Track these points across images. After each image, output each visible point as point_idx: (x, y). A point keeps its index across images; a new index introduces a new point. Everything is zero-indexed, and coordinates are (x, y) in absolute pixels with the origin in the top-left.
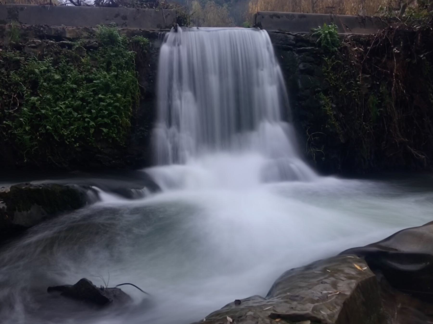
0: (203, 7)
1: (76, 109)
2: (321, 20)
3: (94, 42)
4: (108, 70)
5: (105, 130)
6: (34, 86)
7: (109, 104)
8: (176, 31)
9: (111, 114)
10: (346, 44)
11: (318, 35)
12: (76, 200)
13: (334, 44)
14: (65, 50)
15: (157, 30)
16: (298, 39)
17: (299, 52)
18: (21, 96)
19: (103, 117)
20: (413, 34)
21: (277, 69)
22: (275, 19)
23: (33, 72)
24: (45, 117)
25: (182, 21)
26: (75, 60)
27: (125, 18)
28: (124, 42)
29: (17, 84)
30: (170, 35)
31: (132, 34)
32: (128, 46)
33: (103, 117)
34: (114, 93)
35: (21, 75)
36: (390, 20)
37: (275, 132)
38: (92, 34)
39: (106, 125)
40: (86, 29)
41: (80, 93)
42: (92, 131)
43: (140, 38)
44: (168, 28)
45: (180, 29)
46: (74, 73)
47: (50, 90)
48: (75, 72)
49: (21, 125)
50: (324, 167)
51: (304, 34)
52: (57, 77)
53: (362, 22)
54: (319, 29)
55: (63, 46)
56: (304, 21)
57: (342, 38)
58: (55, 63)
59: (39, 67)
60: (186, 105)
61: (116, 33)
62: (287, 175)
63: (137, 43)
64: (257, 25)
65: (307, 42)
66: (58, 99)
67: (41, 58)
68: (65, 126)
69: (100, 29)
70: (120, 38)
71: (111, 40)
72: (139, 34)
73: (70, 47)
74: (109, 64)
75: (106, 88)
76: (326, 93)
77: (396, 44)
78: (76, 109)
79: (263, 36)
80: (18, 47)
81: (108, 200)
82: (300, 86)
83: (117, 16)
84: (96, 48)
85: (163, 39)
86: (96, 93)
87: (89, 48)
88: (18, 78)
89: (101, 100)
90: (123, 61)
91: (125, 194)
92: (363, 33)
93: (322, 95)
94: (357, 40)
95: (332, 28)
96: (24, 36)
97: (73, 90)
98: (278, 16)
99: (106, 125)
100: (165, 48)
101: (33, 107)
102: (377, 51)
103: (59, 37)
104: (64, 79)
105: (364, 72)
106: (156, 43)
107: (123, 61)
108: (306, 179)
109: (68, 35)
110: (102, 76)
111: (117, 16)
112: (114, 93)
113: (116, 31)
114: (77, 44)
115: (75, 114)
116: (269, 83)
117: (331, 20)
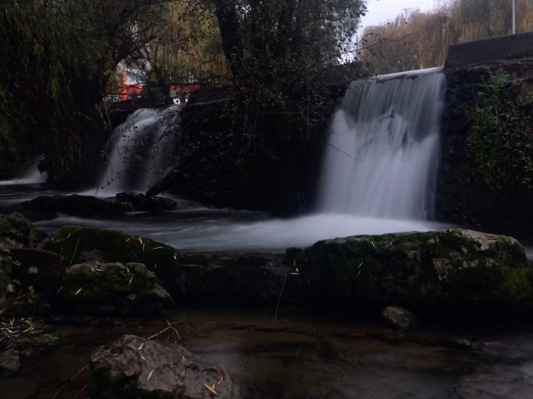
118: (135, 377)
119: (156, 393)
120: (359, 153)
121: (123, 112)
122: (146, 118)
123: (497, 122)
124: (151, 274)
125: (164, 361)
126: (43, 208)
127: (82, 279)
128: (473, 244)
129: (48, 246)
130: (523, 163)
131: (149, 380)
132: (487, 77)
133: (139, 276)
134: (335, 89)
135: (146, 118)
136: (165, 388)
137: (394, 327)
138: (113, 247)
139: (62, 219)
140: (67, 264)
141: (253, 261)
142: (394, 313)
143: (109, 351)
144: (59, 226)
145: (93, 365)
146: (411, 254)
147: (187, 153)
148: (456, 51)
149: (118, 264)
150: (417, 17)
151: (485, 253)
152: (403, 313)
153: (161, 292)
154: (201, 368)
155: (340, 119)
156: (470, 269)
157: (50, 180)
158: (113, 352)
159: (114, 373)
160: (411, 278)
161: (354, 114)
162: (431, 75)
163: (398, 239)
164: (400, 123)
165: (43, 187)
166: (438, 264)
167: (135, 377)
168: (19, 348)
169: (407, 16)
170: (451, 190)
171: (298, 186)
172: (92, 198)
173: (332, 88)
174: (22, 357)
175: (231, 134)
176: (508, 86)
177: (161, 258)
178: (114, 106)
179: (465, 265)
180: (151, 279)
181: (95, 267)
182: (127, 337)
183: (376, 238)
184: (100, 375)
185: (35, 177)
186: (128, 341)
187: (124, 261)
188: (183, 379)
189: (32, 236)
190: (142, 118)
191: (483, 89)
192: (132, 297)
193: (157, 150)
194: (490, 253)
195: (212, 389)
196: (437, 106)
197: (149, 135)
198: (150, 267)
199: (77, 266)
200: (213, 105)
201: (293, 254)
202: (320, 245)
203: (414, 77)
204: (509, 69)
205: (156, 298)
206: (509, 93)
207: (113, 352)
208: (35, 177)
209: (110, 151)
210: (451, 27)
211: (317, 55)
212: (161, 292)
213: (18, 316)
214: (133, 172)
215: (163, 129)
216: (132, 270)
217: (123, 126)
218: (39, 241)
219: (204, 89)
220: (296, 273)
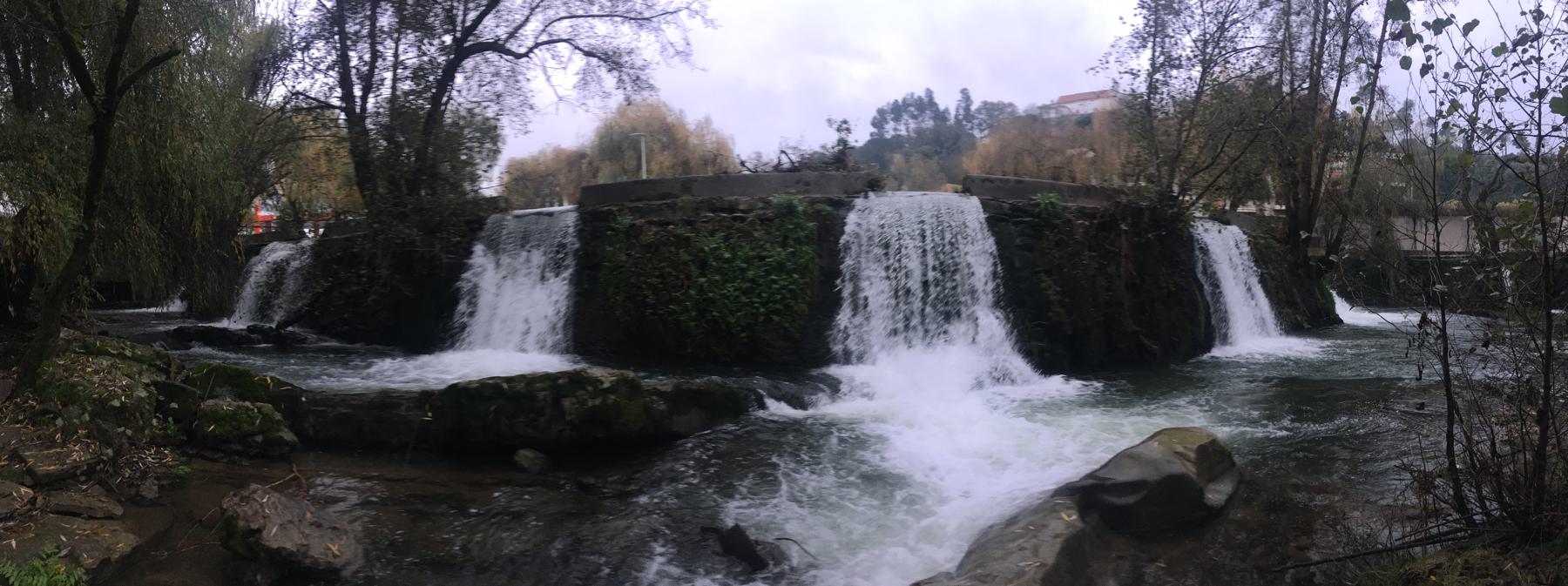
0: (907, 161)
1: (745, 292)
2: (1041, 188)
3: (770, 213)
4: (784, 245)
5: (776, 318)
6: (703, 266)
7: (783, 287)
8: (866, 197)
9: (784, 298)
10: (1070, 216)
11: (1038, 205)
12: (736, 406)
13: (1056, 215)
14: (737, 225)
15: (843, 196)
16: (1014, 208)
17: (1016, 224)
18: (688, 277)
19: (775, 302)
20: (1140, 210)
21: (990, 244)
22: (988, 184)
23: (702, 250)
24: (712, 301)
25: (875, 185)
26: (747, 235)
27: (807, 184)
28: (804, 212)
29: (686, 263)
30: (859, 202)
31: (813, 202)
32: (809, 216)
33: (775, 302)
34: (789, 273)
35: (690, 254)
36: (1120, 191)
37: (992, 324)
38: (768, 203)
39: (777, 312)
40: (762, 200)
41: (750, 274)
42: (761, 318)
43: (823, 206)
44: (856, 194)
45: (871, 194)
46: (746, 250)
47: (719, 271)
48: (747, 249)
49: (686, 310)
50: (1046, 366)
51: (1021, 202)
52: (727, 255)
53: (1088, 191)
54: (1038, 198)
55: (735, 219)
56: (1020, 188)
57: (1065, 208)
58: (726, 239)
59: (710, 244)
60: (876, 289)
61: (796, 202)
62: (1002, 377)
63: (819, 212)
64: (967, 191)
65: (1026, 213)
66: (726, 281)
67: (712, 234)
68: (732, 313)
69: (776, 199)
70: (800, 208)
71: (790, 209)
72: (821, 201)
73: (743, 219)
74: (786, 238)
75: (780, 268)
76: (1048, 273)
77: (1124, 220)
78: (745, 292)
79: (975, 201)
80: (689, 223)
81: (778, 409)
82: (1017, 264)
83: (798, 182)
84: (770, 220)
85: (850, 207)
86: (768, 273)
87: (764, 221)
88: (686, 257)
89: (774, 282)
90: (802, 234)
91: (799, 403)
92: (1089, 204)
93: (1043, 277)
94: (1082, 213)
95: (1053, 197)
96: (696, 210)
97: (743, 270)
98: (992, 181)
99: (777, 312)
100: (852, 218)
101: (701, 290)
102: (1104, 225)
103: (732, 209)
104: (735, 257)
105: (1091, 249)
106: (841, 213)
107: (802, 234)
108: (1027, 382)
109: (742, 207)
110: (777, 253)
111: (798, 182)
112: (789, 273)
113: (796, 199)
114: (751, 216)
115: (744, 299)
116: (979, 258)
117: (1052, 188)
118: (259, 531)
119: (280, 550)
120: (499, 286)
121: (255, 247)
122: (278, 251)
123: (624, 258)
124: (278, 416)
125: (288, 517)
126: (182, 338)
127: (215, 417)
128: (597, 382)
129: (187, 380)
130: (646, 297)
131: (274, 537)
132: (615, 219)
133: (266, 418)
134: (472, 222)
135: (278, 251)
136: (288, 546)
137: (525, 470)
138: (241, 383)
139: (198, 349)
140: (202, 399)
141: (387, 401)
142: (525, 456)
143: (237, 499)
144: (196, 357)
145: (224, 511)
146: (541, 395)
147: (319, 290)
148: (587, 191)
149: (247, 404)
150: (558, 153)
151: (607, 391)
152: (882, 426)
153: (288, 436)
154: (326, 525)
155: (479, 249)
156: (594, 407)
157: (189, 308)
158: (241, 500)
159: (241, 523)
160: (542, 419)
161: (494, 247)
162: (566, 212)
163: (529, 380)
164: (538, 258)
165: (182, 316)
166: (567, 403)
167: (259, 531)
168: (158, 478)
169: (549, 151)
170: (584, 329)
171: (434, 319)
172: (225, 330)
173: (468, 223)
174: (161, 488)
175: (14, 543)
176: (632, 226)
177: (289, 400)
178: (251, 237)
179: (590, 403)
180: (278, 422)
181: (227, 404)
182: (254, 486)
183: (508, 380)
184: (228, 525)
185: (176, 306)
186: (254, 492)
187: (254, 400)
188: (307, 537)
189: (173, 369)
190: (273, 251)
191: (612, 229)
192: (259, 439)
193: (291, 285)
194: (613, 389)
195: (334, 549)
196: (573, 243)
197: (279, 269)
198: (277, 408)
199: (210, 402)
200: (347, 239)
201: (426, 398)
202: (454, 389)
203: (550, 214)
204: (633, 211)
205: (282, 442)
206: (633, 232)
207: (241, 500)
208: (176, 306)
209: (242, 286)
210: (590, 163)
211: (456, 187)
212: (288, 436)
213: (159, 446)
214: (263, 307)
215: (295, 264)
216: (259, 409)
217: (255, 259)
218: (178, 373)
219: (336, 224)
220: (429, 417)
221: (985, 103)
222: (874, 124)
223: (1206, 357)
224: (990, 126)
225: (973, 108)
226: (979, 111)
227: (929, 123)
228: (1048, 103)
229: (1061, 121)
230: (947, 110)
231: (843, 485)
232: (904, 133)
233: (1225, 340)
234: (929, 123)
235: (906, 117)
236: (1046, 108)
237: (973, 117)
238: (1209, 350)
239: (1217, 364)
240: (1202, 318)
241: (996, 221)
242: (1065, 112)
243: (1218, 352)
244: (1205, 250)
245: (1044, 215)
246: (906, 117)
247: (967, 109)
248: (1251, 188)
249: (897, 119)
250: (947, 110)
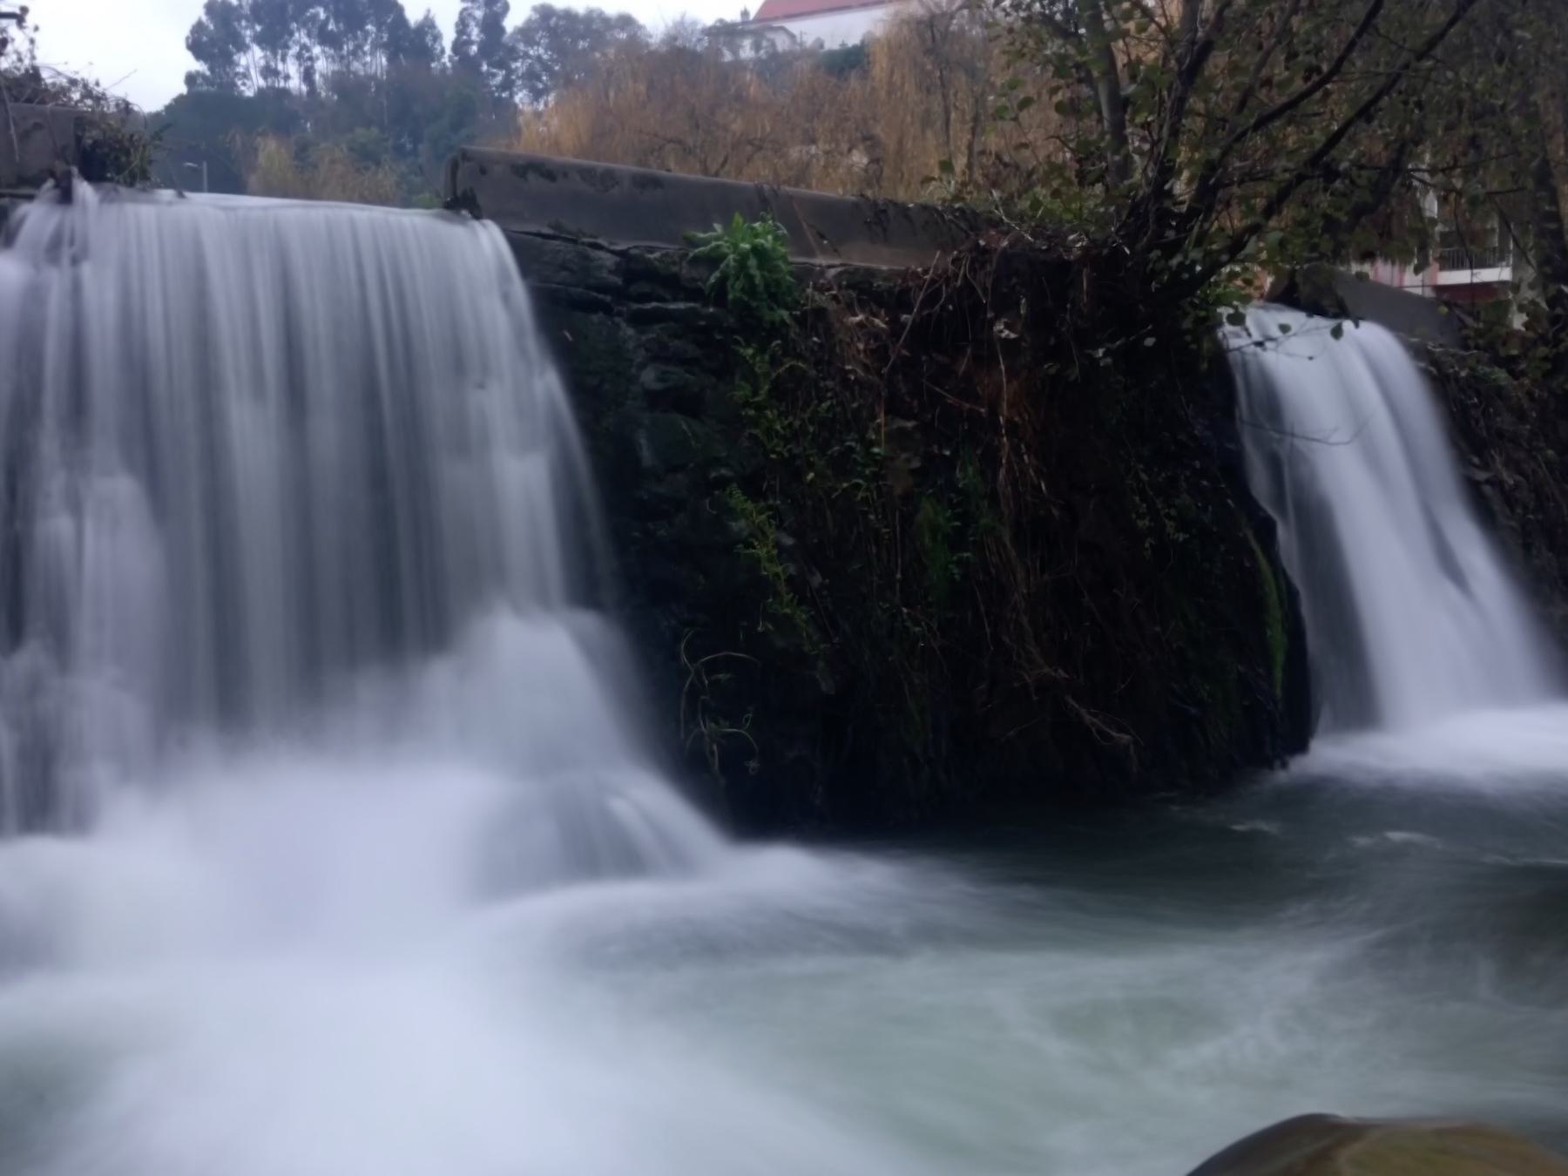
8: (66, 196)
10: (822, 299)
11: (713, 260)
16: (633, 269)
17: (641, 320)
21: (548, 384)
45: (84, 190)
50: (754, 804)
51: (658, 251)
54: (715, 236)
56: (650, 201)
62: (597, 850)
64: (462, 202)
76: (753, 488)
77: (1005, 306)
82: (647, 456)
92: (883, 261)
93: (737, 499)
94: (862, 289)
95: (766, 233)
108: (680, 862)
116: (515, 453)
221: (545, 13)
222: (197, 45)
223: (1281, 777)
224: (566, 81)
225: (513, 21)
226: (526, 33)
227: (376, 63)
228: (733, 16)
229: (775, 66)
230: (428, 25)
231: (1121, 105)
232: (295, 84)
233: (1363, 710)
234: (376, 63)
235: (301, 36)
236: (726, 32)
237: (512, 53)
238: (1300, 745)
239: (1316, 790)
240: (1276, 635)
241: (574, 305)
242: (782, 43)
243: (1332, 754)
244: (1271, 405)
245: (734, 293)
246: (301, 36)
247: (492, 25)
248: (1377, 219)
249: (274, 40)
250: (428, 25)
